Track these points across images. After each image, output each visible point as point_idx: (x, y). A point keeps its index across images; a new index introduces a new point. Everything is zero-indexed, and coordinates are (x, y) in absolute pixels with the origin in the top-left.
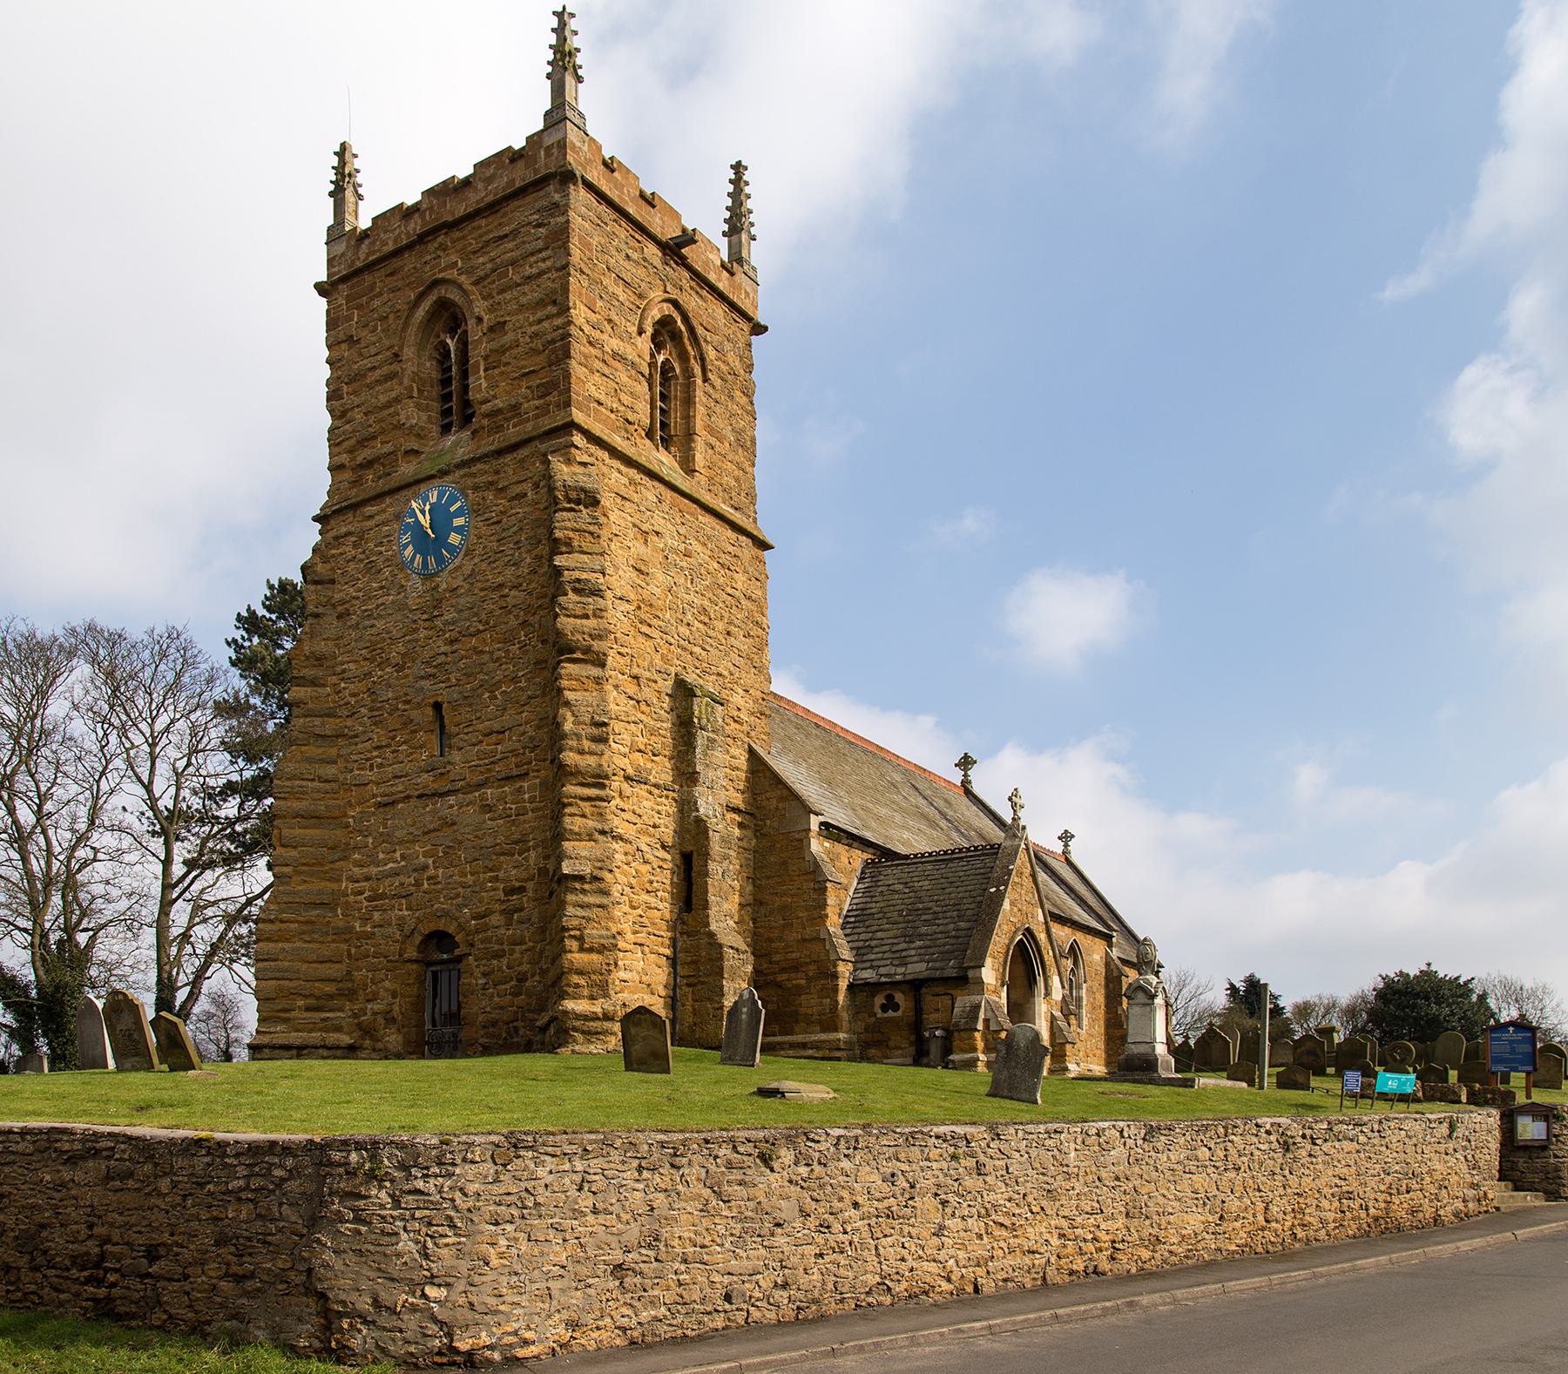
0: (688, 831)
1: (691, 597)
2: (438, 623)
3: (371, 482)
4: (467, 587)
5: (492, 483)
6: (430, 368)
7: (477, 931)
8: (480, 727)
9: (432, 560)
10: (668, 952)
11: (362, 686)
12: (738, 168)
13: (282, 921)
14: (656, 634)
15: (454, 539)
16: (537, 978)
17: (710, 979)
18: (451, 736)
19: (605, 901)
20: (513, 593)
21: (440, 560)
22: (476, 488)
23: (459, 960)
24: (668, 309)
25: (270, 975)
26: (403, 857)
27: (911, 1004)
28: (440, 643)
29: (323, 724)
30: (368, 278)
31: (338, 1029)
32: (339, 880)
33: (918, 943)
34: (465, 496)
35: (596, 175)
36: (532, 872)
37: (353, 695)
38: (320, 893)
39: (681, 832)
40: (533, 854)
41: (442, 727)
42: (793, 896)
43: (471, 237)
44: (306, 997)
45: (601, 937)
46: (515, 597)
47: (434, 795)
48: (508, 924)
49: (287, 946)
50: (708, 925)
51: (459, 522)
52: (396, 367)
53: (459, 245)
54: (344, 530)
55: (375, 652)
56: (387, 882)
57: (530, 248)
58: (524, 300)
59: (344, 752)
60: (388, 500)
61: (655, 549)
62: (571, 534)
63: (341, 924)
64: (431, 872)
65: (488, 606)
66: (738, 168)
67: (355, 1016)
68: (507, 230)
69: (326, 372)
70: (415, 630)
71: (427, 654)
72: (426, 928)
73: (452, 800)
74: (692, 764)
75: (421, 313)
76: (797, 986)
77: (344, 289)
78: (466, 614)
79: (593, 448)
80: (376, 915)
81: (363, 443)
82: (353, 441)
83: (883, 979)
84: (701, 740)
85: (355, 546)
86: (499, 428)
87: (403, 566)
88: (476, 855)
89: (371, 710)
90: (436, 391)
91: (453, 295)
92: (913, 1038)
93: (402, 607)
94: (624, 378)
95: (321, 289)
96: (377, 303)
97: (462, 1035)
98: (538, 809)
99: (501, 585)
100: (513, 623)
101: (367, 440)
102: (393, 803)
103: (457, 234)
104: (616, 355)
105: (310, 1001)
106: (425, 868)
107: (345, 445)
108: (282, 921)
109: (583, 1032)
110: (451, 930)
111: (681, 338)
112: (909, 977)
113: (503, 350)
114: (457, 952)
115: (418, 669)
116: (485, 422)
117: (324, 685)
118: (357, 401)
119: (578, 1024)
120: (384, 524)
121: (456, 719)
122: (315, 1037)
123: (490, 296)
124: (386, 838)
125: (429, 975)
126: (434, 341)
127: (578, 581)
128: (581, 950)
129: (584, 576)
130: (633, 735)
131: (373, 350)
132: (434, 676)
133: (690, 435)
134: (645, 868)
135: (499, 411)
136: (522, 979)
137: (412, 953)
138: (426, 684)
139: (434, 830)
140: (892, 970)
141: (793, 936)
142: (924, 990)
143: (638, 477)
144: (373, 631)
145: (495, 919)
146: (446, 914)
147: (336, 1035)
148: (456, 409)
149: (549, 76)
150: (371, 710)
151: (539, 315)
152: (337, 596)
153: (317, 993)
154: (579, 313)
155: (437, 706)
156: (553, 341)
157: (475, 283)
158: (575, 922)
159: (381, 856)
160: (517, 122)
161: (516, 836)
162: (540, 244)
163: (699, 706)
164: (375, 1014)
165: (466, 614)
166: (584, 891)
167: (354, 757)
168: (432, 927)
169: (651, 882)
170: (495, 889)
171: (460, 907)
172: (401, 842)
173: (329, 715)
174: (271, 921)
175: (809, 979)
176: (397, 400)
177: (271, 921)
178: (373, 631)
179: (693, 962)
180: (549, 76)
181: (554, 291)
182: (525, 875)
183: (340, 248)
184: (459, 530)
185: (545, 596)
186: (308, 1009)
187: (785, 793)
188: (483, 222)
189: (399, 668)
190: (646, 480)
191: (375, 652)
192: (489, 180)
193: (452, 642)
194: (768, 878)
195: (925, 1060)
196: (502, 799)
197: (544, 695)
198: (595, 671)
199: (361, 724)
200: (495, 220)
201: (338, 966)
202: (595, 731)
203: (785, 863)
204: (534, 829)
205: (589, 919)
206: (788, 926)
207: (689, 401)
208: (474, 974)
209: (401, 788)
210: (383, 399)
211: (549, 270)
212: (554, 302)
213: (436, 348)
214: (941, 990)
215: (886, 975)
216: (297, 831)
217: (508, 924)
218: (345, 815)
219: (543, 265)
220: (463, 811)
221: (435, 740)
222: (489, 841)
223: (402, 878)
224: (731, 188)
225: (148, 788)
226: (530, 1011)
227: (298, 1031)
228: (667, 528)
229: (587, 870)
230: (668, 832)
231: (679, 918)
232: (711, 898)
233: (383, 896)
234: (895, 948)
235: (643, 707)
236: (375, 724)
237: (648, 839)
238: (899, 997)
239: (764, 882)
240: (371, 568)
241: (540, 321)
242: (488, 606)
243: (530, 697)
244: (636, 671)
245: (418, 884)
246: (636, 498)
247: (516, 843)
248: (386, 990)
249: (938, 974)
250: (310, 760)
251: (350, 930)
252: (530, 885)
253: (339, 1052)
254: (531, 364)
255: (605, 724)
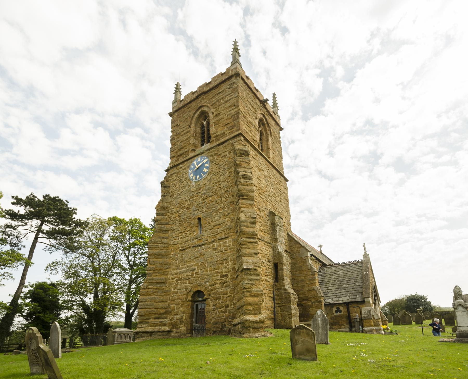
0: (276, 256)
1: (271, 189)
2: (200, 194)
3: (181, 160)
4: (209, 183)
5: (216, 154)
6: (198, 129)
7: (211, 290)
8: (212, 224)
9: (198, 177)
10: (272, 295)
11: (177, 215)
12: (274, 94)
13: (148, 289)
14: (264, 198)
15: (205, 170)
16: (232, 306)
17: (286, 304)
18: (203, 227)
19: (258, 278)
20: (223, 183)
21: (201, 176)
22: (211, 156)
23: (205, 300)
24: (262, 116)
25: (143, 307)
26: (188, 267)
27: (346, 310)
28: (200, 200)
29: (165, 227)
30: (182, 110)
31: (165, 325)
32: (167, 275)
33: (344, 290)
34: (209, 158)
35: (245, 78)
36: (230, 269)
37: (174, 218)
38: (161, 279)
39: (274, 256)
40: (230, 263)
41: (200, 225)
42: (304, 277)
43: (210, 95)
44: (155, 314)
45: (258, 291)
46: (224, 184)
47: (198, 246)
48: (222, 287)
49: (149, 297)
50: (284, 286)
51: (206, 165)
52: (189, 129)
53: (207, 98)
54: (173, 172)
55: (181, 205)
56: (182, 275)
57: (227, 94)
58: (225, 107)
59: (170, 235)
60: (186, 163)
61: (262, 174)
62: (241, 163)
63: (167, 289)
64: (196, 271)
65: (215, 188)
66: (274, 94)
67: (170, 320)
68: (220, 91)
69: (171, 134)
70: (193, 197)
71: (196, 204)
72: (194, 290)
73: (203, 247)
74: (275, 235)
75: (196, 115)
76: (308, 305)
77: (176, 114)
78: (208, 191)
79: (246, 143)
80: (179, 286)
81: (179, 150)
82: (177, 150)
83: (335, 302)
84: (278, 228)
85: (176, 176)
86: (219, 140)
87: (189, 180)
88: (211, 264)
89: (179, 222)
90: (200, 135)
91: (205, 109)
92: (348, 322)
93: (189, 191)
94: (252, 129)
95: (171, 115)
96: (185, 115)
97: (206, 327)
98: (232, 248)
99: (219, 181)
100: (223, 191)
101: (181, 149)
102: (185, 249)
103: (206, 95)
104: (250, 122)
105: (157, 316)
106: (194, 270)
107: (175, 151)
108: (148, 289)
109: (253, 328)
110: (202, 290)
111: (265, 125)
112: (345, 301)
113: (219, 120)
114: (205, 298)
115: (193, 208)
116: (214, 139)
117: (165, 216)
118: (178, 140)
119: (251, 325)
120: (185, 169)
121: (205, 222)
122: (157, 328)
123: (216, 108)
124: (182, 261)
125: (195, 305)
126: (200, 123)
127: (244, 175)
128: (251, 296)
129: (246, 174)
130: (259, 226)
131: (183, 126)
132: (198, 210)
133: (268, 149)
134: (264, 268)
135: (218, 135)
136: (227, 307)
137: (190, 298)
138: (196, 212)
139: (198, 257)
140: (338, 299)
141: (306, 289)
142: (350, 306)
143: (258, 154)
144: (181, 199)
145: (217, 286)
146: (201, 285)
147: (164, 327)
148: (205, 137)
149: (232, 55)
150: (179, 222)
151: (230, 109)
152: (171, 190)
153: (158, 312)
154: (241, 108)
155: (199, 219)
156: (234, 115)
157: (212, 106)
158: (248, 286)
159: (181, 266)
160: (222, 66)
161: (224, 258)
162: (230, 92)
163: (277, 219)
164: (177, 319)
165: (208, 191)
166: (251, 275)
167: (173, 236)
168: (197, 289)
169: (266, 272)
170: (217, 276)
171: (206, 282)
172: (187, 262)
173: (166, 224)
174: (145, 289)
175: (312, 303)
176: (189, 138)
177: (145, 289)
178: (181, 199)
179: (280, 299)
180: (232, 55)
181: (234, 103)
182: (227, 270)
183: (176, 104)
184: (206, 167)
185: (233, 183)
186: (155, 318)
187: (299, 246)
188: (214, 91)
189: (188, 208)
190: (259, 155)
191: (181, 205)
192: (216, 81)
193: (204, 199)
194: (296, 271)
195: (353, 329)
196: (219, 246)
197: (233, 212)
198: (251, 202)
199: (176, 226)
200: (217, 89)
201: (165, 303)
202: (252, 220)
203: (301, 267)
204: (230, 255)
205: (253, 285)
206: (303, 286)
207: (267, 141)
208: (210, 306)
209: (187, 245)
210: (185, 138)
211: (232, 98)
212: (234, 106)
213: (200, 125)
214: (355, 305)
215: (336, 301)
216: (155, 260)
217: (222, 287)
218: (170, 254)
219: (230, 97)
220: (208, 251)
221: (198, 229)
222: (215, 260)
223: (187, 273)
224: (273, 98)
225: (128, 257)
226: (230, 318)
227: (151, 326)
228: (265, 169)
229: (251, 267)
230: (269, 257)
231: (274, 284)
232: (285, 278)
233: (181, 279)
234: (336, 292)
235: (262, 218)
236: (180, 226)
237: (264, 259)
238: (341, 308)
239: (295, 273)
240: (181, 181)
241: (230, 111)
242: (215, 188)
243: (229, 213)
244: (259, 207)
245: (192, 275)
246: (257, 159)
247: (224, 260)
248: (181, 311)
249: (354, 300)
250: (160, 238)
251: (170, 291)
252: (229, 274)
253: (165, 333)
254: (229, 121)
255: (255, 218)
